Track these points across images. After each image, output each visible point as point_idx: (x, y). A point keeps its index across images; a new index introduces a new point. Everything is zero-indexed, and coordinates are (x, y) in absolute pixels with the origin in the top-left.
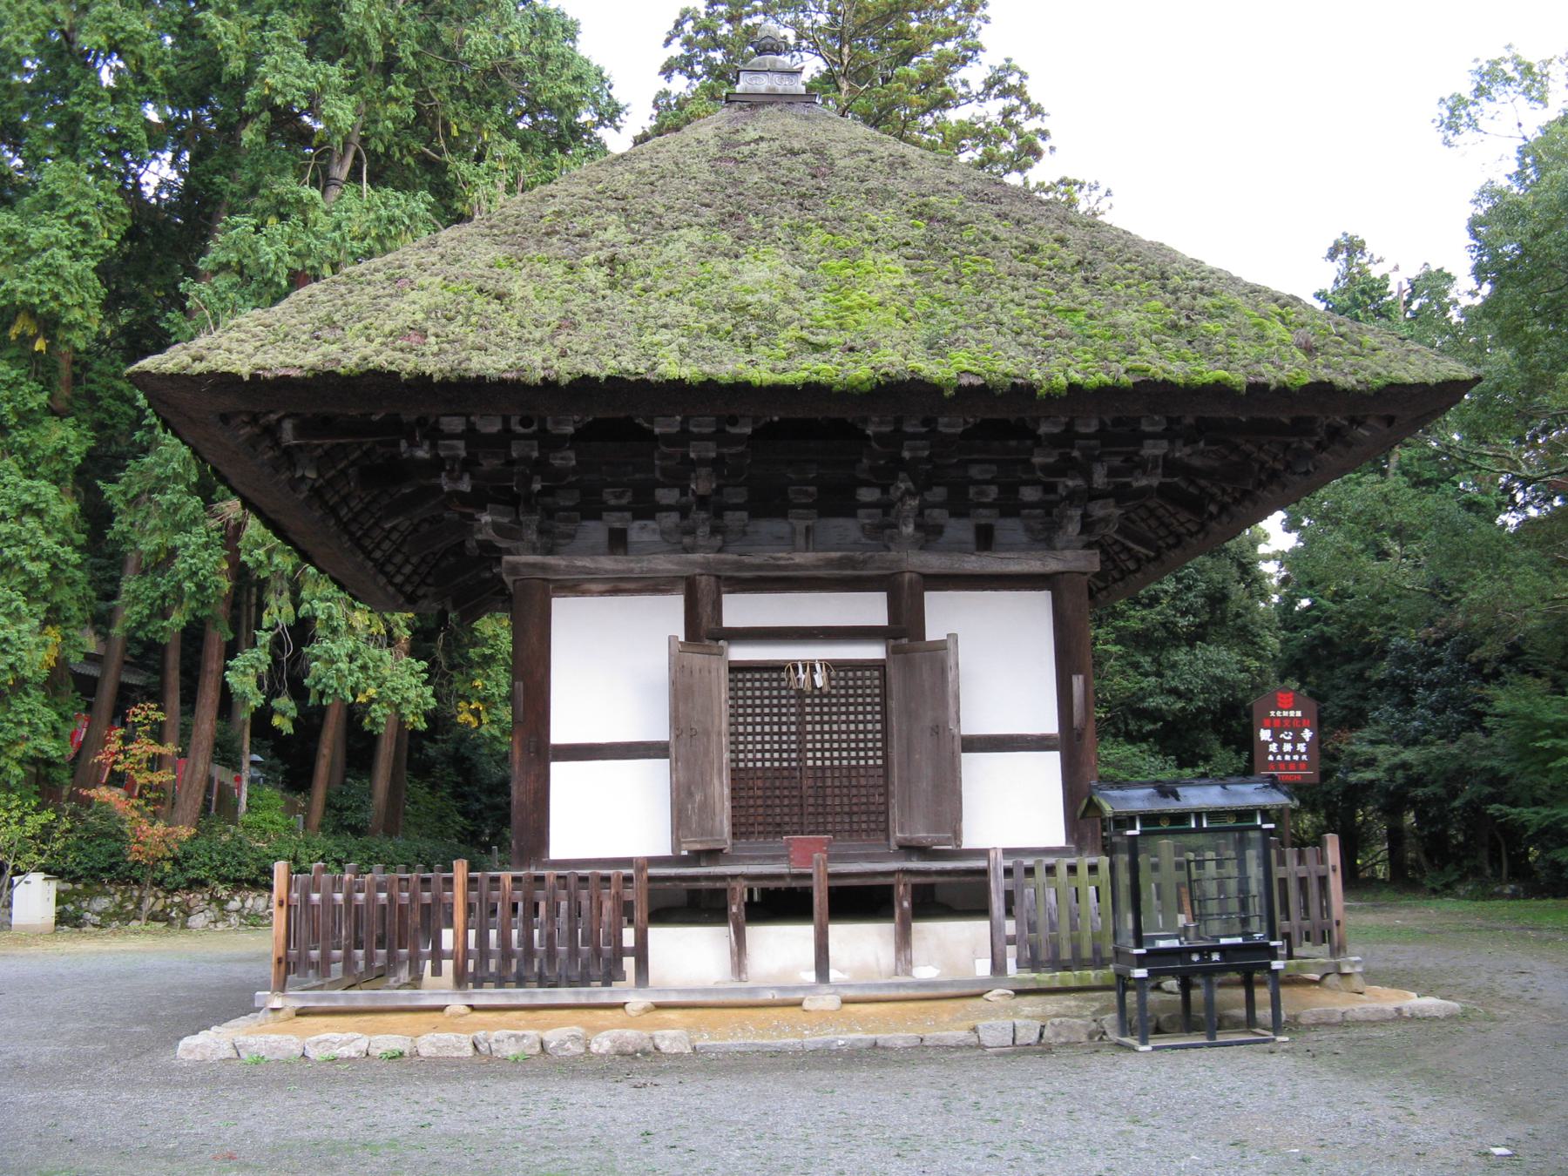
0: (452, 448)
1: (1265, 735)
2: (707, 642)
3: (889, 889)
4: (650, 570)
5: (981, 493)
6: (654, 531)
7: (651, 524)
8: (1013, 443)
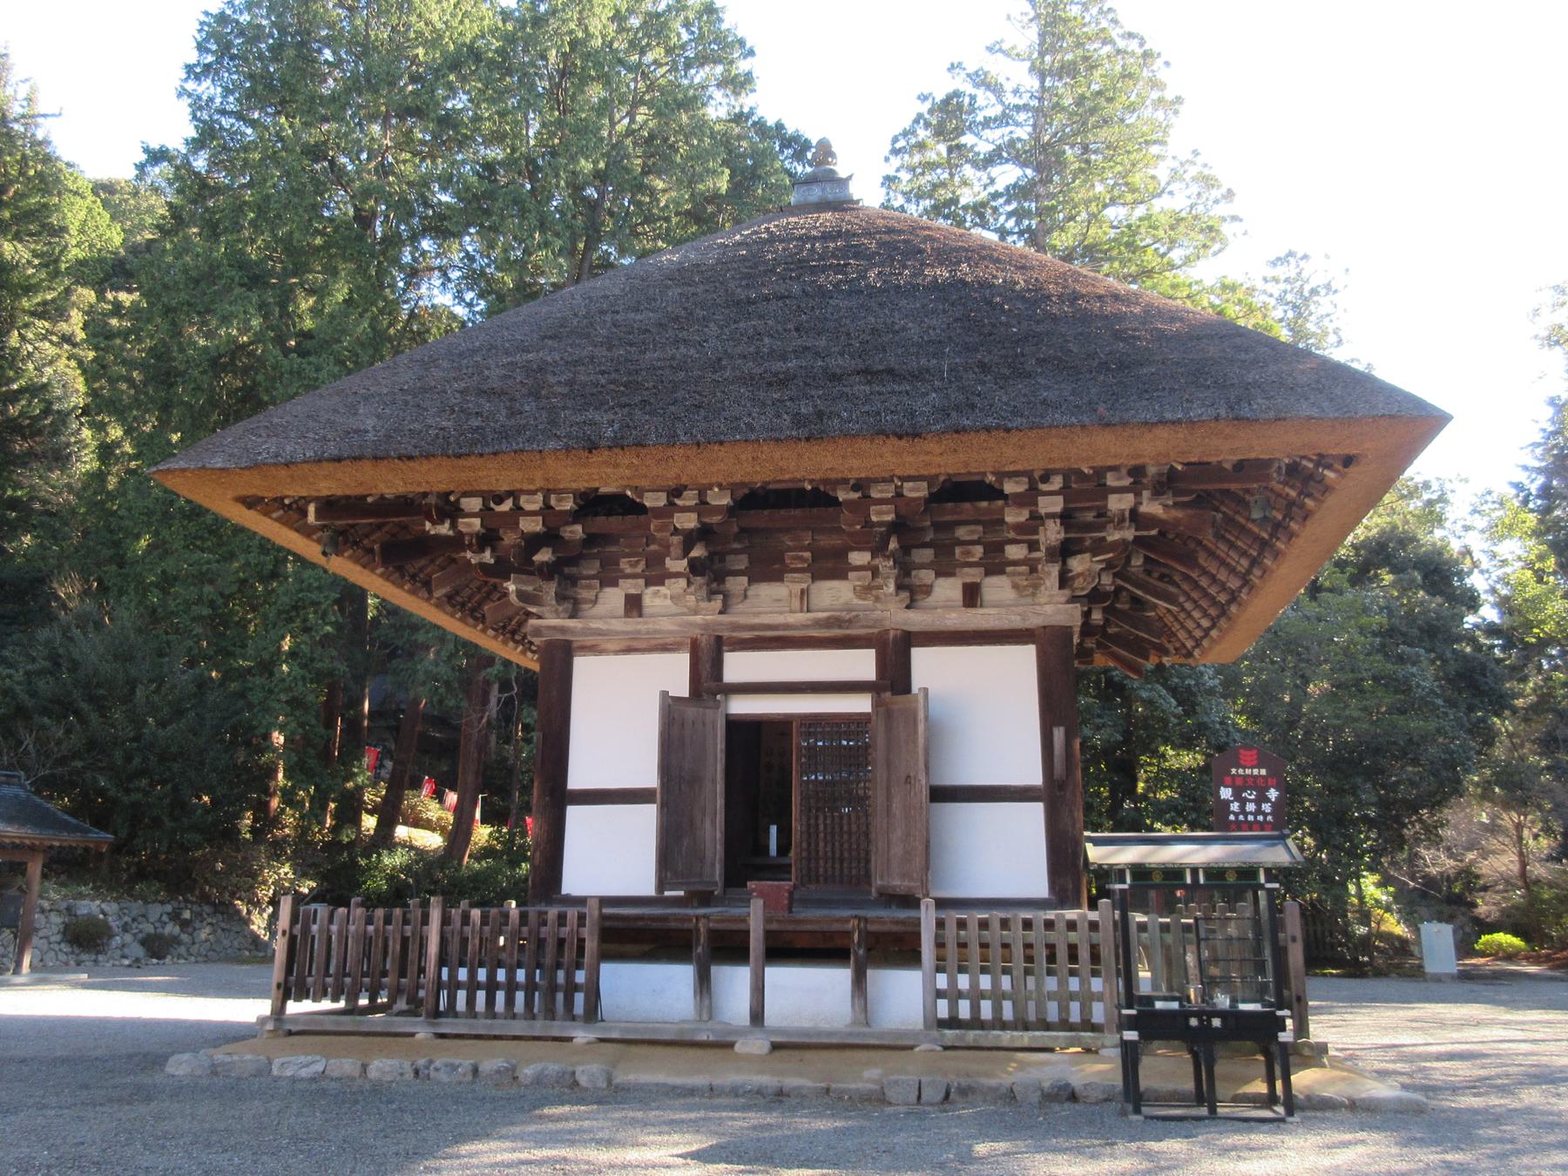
0: (469, 525)
1: (1226, 793)
4: (656, 632)
5: (968, 553)
6: (665, 596)
8: (984, 504)
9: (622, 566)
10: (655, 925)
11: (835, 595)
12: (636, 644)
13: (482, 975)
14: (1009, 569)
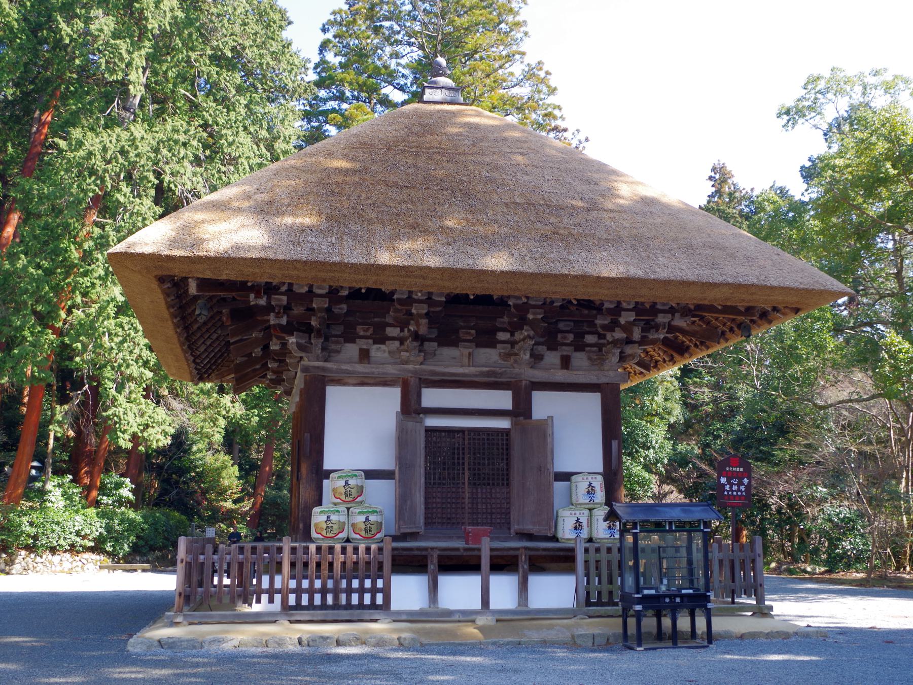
0: (279, 300)
2: (414, 415)
3: (516, 557)
4: (383, 374)
5: (565, 338)
7: (383, 347)
9: (358, 330)
10: (405, 553)
11: (489, 357)
12: (367, 380)
13: (368, 584)
14: (588, 349)
